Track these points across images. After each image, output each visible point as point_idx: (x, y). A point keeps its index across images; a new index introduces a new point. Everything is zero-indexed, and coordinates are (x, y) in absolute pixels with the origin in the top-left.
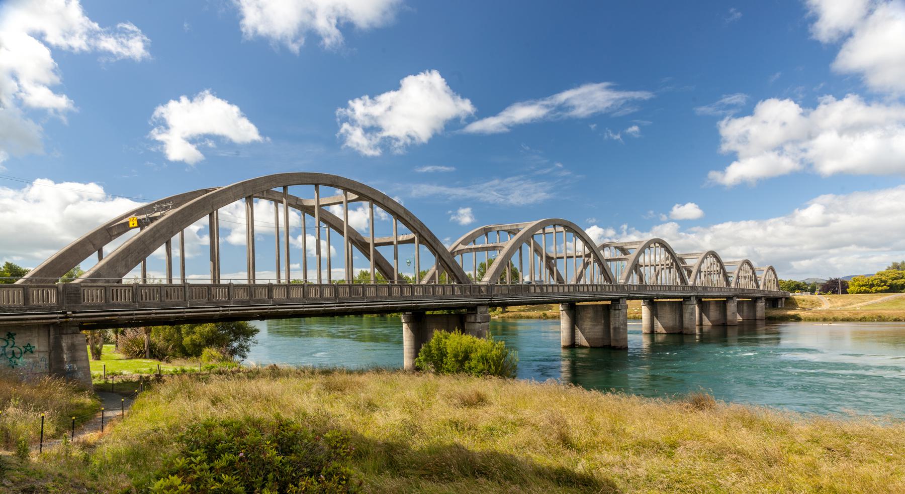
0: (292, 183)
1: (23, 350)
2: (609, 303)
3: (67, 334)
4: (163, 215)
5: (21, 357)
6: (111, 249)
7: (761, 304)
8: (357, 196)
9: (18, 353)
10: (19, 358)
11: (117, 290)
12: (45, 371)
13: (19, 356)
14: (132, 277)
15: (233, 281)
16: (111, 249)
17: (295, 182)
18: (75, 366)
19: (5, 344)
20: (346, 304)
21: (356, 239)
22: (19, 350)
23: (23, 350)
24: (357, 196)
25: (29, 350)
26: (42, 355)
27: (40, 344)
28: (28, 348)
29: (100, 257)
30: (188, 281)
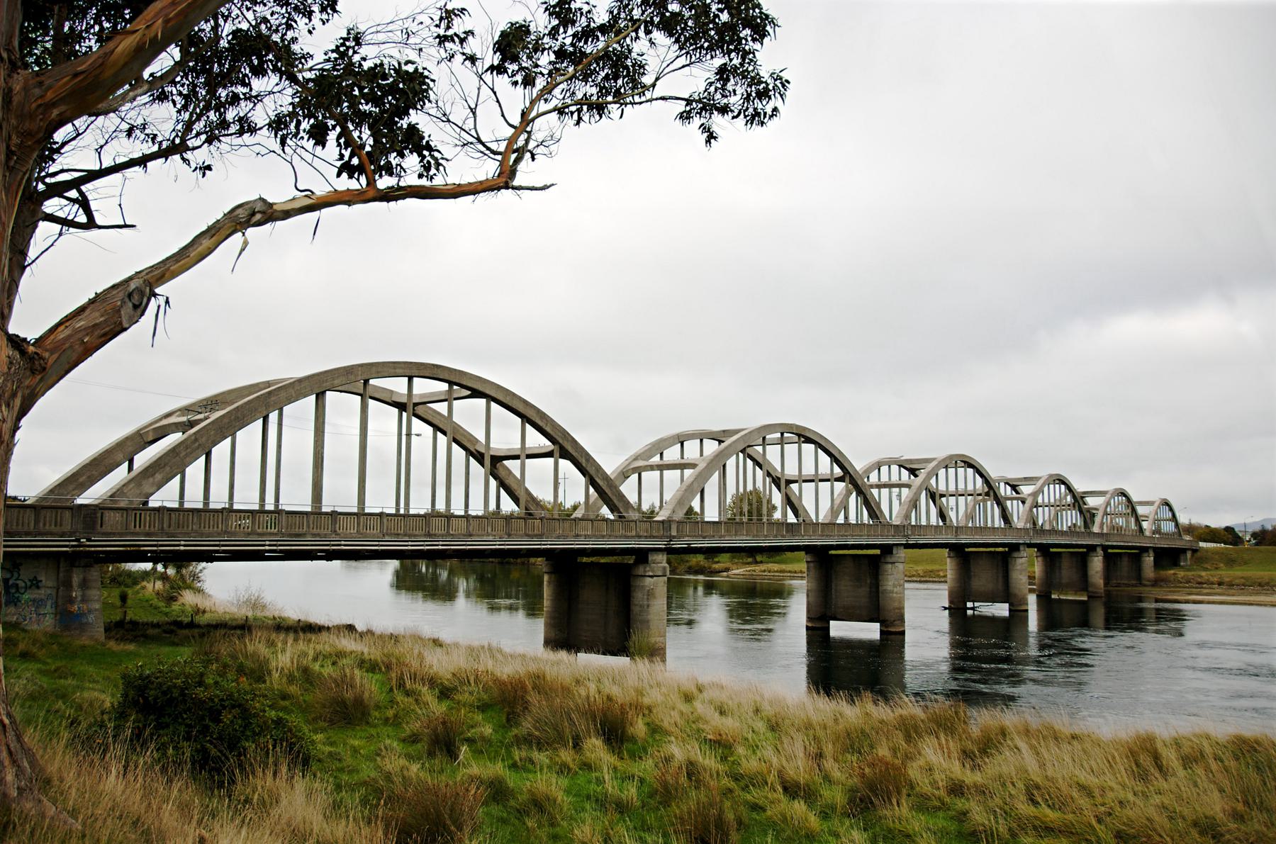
0: (373, 376)
1: (29, 584)
2: (878, 552)
3: (79, 567)
4: (206, 418)
5: (25, 591)
6: (143, 459)
7: (1148, 559)
8: (469, 392)
9: (22, 588)
10: (23, 594)
11: (141, 514)
12: (51, 611)
13: (23, 591)
14: (165, 497)
15: (337, 509)
16: (143, 459)
17: (380, 376)
18: (85, 607)
19: (8, 576)
20: (441, 543)
21: (477, 451)
22: (23, 584)
23: (29, 584)
24: (469, 392)
25: (35, 584)
26: (49, 591)
27: (48, 581)
28: (34, 582)
29: (130, 469)
30: (470, 513)
